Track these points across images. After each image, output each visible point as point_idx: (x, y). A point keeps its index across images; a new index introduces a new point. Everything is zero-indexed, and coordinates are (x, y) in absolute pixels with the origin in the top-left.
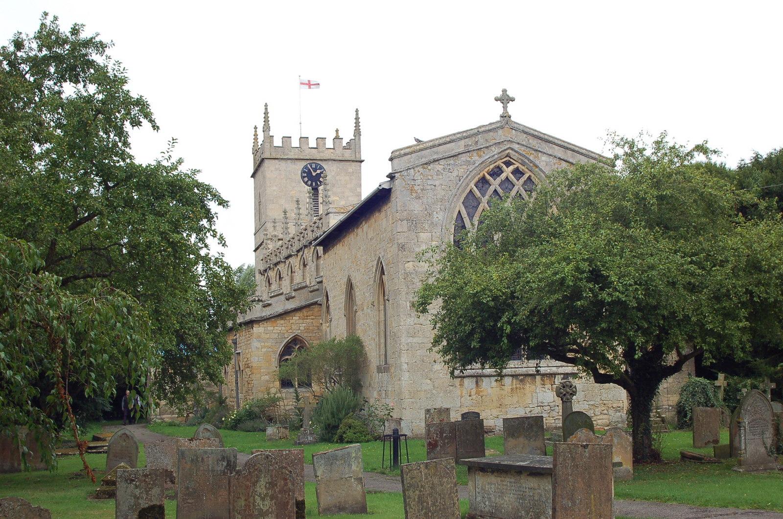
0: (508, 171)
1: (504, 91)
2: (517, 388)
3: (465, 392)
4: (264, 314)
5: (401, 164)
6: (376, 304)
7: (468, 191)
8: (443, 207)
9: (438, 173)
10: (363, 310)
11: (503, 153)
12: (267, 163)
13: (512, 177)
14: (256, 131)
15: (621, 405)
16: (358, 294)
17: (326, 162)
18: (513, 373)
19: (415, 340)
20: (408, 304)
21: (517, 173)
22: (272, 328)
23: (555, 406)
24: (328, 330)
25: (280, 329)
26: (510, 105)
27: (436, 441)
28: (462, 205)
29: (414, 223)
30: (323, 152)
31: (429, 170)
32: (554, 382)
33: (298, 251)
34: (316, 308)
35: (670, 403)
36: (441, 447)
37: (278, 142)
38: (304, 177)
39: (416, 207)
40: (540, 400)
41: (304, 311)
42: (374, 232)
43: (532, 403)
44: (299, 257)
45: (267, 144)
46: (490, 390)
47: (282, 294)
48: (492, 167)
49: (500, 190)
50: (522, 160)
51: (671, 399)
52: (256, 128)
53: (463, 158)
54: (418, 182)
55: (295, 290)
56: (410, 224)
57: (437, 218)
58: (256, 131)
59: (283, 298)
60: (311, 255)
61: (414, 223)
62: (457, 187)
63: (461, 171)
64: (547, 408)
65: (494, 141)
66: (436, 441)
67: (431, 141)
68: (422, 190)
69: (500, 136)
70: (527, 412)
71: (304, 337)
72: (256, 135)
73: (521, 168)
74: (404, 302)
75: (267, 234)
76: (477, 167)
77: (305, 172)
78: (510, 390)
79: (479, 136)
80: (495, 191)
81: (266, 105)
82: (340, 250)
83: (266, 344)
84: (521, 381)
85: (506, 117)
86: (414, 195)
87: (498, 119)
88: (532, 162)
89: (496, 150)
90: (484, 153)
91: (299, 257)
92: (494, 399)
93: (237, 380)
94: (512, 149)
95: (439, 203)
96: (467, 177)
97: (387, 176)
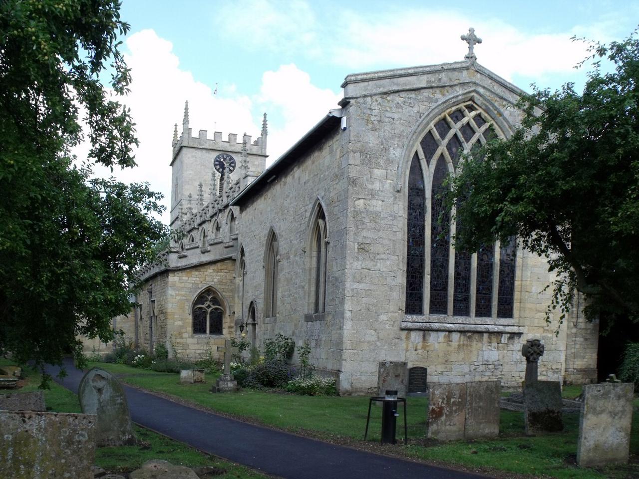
0: (470, 116)
1: (472, 31)
2: (464, 345)
3: (410, 345)
4: (179, 265)
5: (353, 90)
6: (307, 250)
7: (426, 131)
8: (400, 143)
9: (398, 106)
10: (288, 258)
11: (468, 95)
12: (184, 150)
13: (473, 124)
14: (176, 128)
15: (559, 367)
16: (283, 245)
17: (237, 154)
18: (462, 329)
19: (361, 286)
20: (356, 246)
21: (480, 120)
22: (187, 278)
23: (499, 365)
24: (241, 283)
25: (195, 279)
26: (477, 47)
27: (441, 408)
28: (419, 145)
29: (368, 156)
30: (234, 146)
31: (389, 101)
32: (501, 341)
33: (212, 217)
34: (229, 263)
35: (575, 366)
36: (447, 416)
37: (195, 134)
38: (217, 165)
39: (372, 140)
40: (485, 358)
41: (219, 264)
42: (309, 175)
43: (477, 361)
44: (213, 222)
45: (185, 134)
46: (437, 346)
47: (198, 247)
48: (454, 109)
49: (460, 135)
50: (486, 106)
51: (577, 363)
52: (176, 125)
53: (426, 93)
54: (375, 112)
55: (211, 245)
56: (364, 157)
57: (394, 154)
58: (176, 128)
59: (198, 251)
60: (225, 218)
61: (368, 156)
62: (418, 124)
63: (423, 108)
64: (490, 367)
65: (457, 82)
66: (441, 408)
67: (391, 71)
68: (380, 121)
69: (465, 76)
70: (472, 370)
71: (219, 290)
72: (176, 131)
73: (484, 115)
74: (352, 243)
75: (182, 209)
76: (440, 105)
77: (217, 161)
78: (457, 346)
79: (443, 73)
80: (455, 135)
81: (187, 102)
82: (261, 204)
83: (180, 293)
84: (469, 338)
85: (471, 57)
86: (370, 126)
87: (463, 59)
88: (496, 109)
89: (460, 91)
90: (448, 92)
91: (213, 222)
92: (441, 355)
93: (151, 325)
94: (478, 93)
95: (397, 139)
96: (428, 114)
97: (339, 104)
